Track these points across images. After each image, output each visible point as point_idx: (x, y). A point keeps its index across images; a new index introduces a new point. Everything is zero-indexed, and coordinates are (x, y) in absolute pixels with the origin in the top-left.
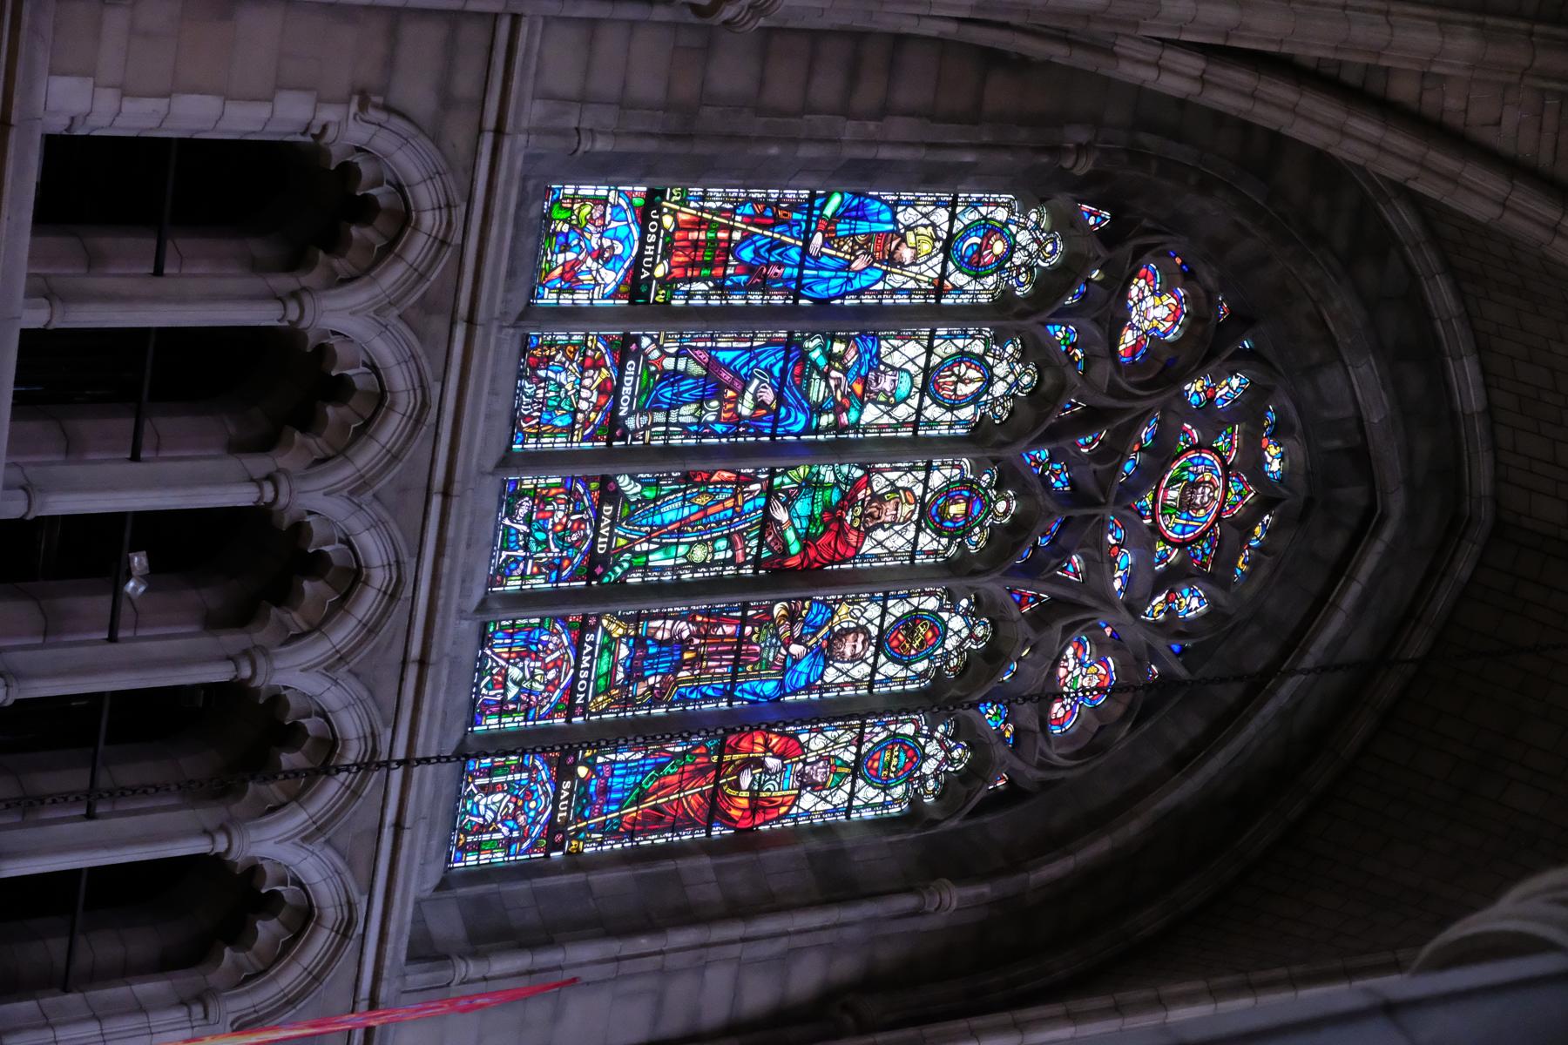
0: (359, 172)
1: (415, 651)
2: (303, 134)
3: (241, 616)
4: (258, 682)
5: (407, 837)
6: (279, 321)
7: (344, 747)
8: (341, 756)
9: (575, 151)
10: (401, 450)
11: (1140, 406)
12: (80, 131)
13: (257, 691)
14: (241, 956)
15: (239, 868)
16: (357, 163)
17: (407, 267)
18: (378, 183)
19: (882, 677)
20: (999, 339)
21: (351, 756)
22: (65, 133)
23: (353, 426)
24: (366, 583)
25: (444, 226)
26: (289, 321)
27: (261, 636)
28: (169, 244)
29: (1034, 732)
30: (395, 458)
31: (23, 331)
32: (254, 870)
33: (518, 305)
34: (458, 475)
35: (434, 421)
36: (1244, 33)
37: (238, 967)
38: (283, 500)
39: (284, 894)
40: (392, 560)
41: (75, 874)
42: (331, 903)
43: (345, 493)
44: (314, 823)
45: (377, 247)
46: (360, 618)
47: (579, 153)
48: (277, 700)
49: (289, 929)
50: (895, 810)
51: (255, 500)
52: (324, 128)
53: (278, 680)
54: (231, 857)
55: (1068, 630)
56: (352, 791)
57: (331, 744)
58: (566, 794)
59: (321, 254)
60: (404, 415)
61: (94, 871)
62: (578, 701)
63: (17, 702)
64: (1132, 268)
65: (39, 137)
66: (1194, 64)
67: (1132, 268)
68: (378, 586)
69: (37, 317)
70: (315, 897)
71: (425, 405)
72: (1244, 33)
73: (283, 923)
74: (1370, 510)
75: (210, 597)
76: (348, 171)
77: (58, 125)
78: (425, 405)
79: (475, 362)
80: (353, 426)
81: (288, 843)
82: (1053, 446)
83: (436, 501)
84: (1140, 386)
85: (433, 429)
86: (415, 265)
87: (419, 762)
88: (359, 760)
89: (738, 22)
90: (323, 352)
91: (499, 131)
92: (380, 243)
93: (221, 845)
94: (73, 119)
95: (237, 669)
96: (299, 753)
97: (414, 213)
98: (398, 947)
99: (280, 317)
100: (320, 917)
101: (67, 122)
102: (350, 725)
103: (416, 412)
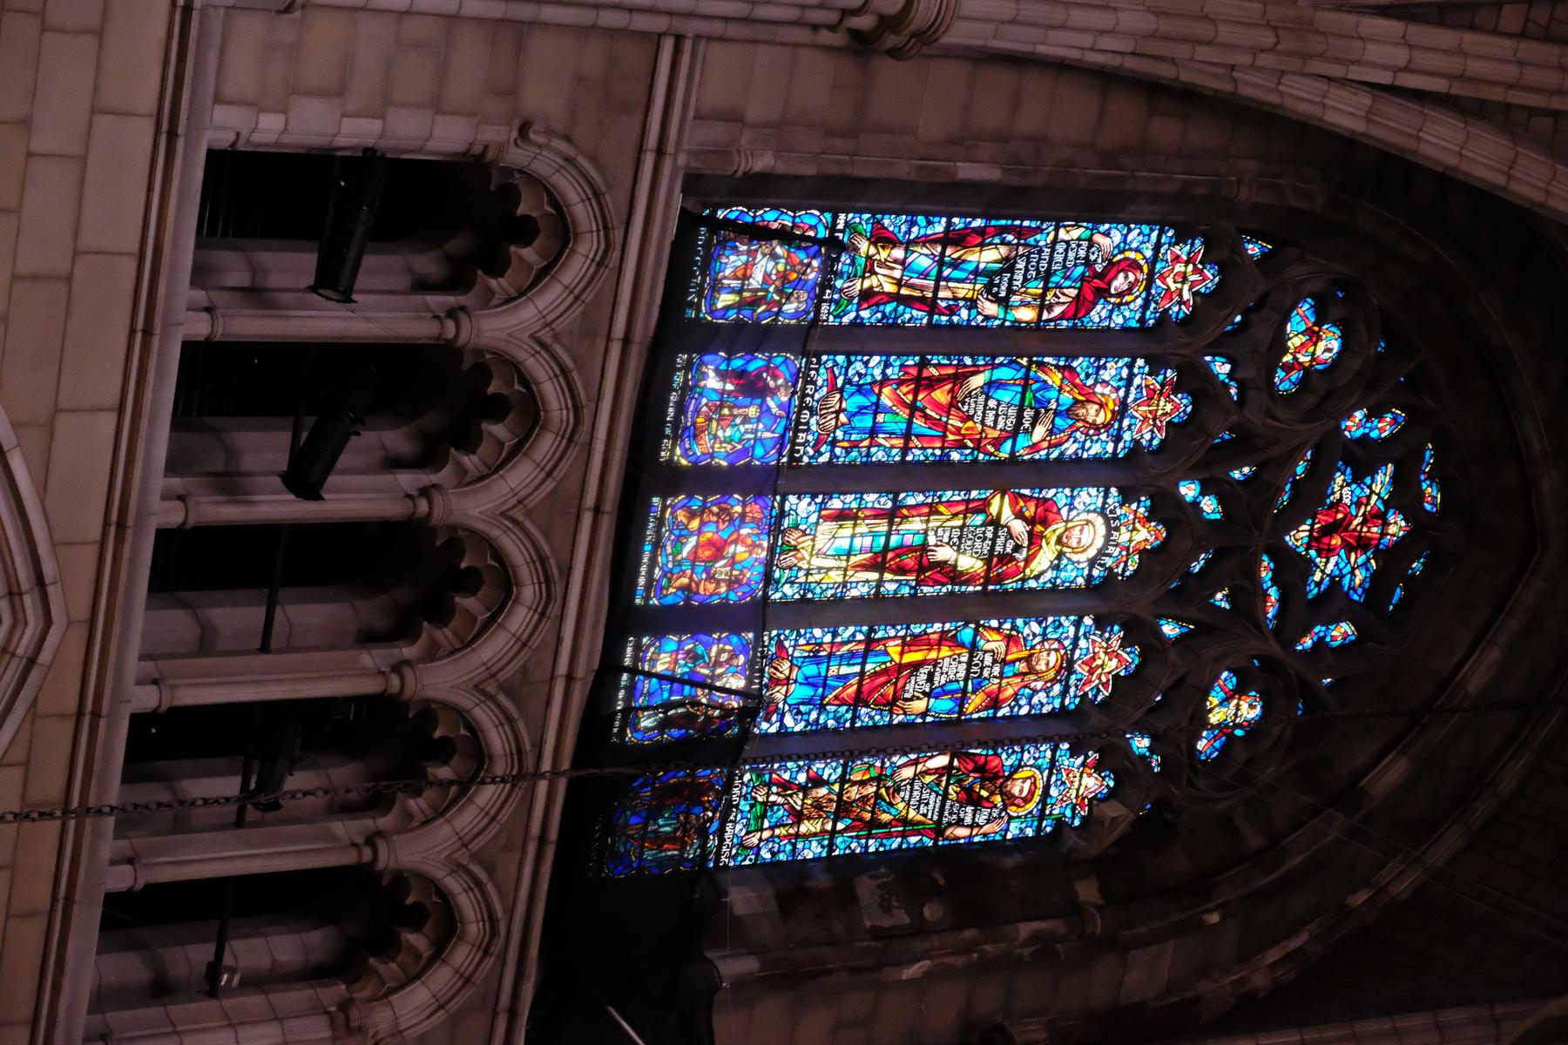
3: (457, 279)
4: (381, 865)
12: (241, 147)
13: (381, 874)
17: (535, 466)
19: (1054, 285)
25: (544, 599)
27: (445, 475)
35: (617, 265)
36: (1376, 118)
39: (428, 906)
42: (502, 752)
46: (513, 632)
49: (516, 436)
52: (486, 148)
57: (479, 754)
63: (149, 887)
65: (127, 717)
68: (528, 603)
71: (494, 932)
72: (1376, 118)
75: (428, 264)
76: (482, 371)
77: (224, 139)
86: (462, 970)
88: (508, 772)
91: (660, 152)
94: (238, 134)
96: (529, 248)
97: (542, 413)
100: (518, 597)
102: (497, 740)
103: (541, 574)
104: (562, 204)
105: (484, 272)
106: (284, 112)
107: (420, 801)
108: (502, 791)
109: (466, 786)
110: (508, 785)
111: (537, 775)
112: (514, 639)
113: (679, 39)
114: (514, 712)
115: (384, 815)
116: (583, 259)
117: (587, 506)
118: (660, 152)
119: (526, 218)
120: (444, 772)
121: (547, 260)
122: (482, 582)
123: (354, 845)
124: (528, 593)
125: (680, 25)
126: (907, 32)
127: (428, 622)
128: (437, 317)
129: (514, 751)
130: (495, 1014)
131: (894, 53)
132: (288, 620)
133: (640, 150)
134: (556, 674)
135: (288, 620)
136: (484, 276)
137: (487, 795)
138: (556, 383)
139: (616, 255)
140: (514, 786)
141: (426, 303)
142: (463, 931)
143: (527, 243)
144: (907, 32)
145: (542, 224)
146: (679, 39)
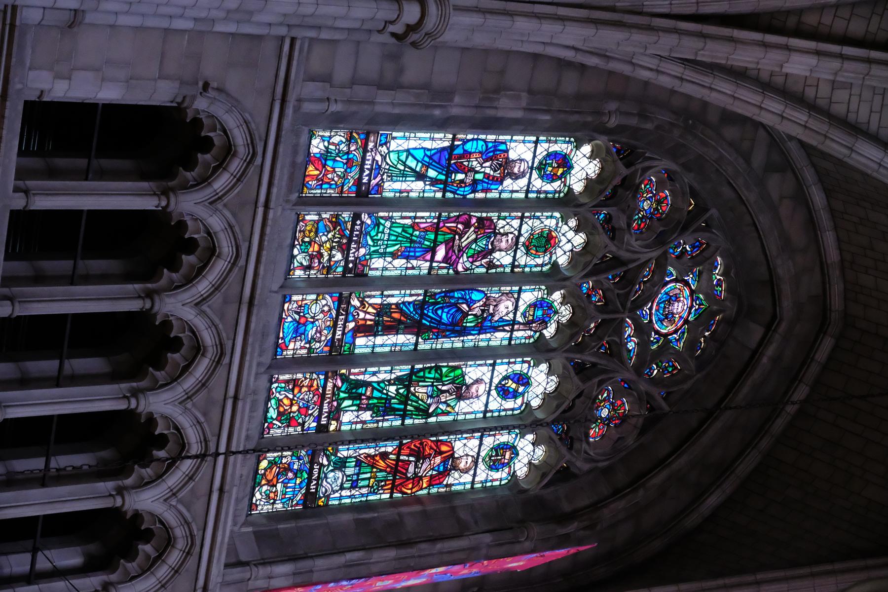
0: (187, 225)
1: (231, 392)
2: (172, 102)
3: (147, 274)
4: (140, 409)
5: (240, 404)
6: (156, 207)
7: (174, 541)
8: (188, 451)
9: (327, 110)
10: (193, 475)
11: (644, 258)
12: (46, 99)
14: (174, 276)
15: (143, 417)
16: (201, 118)
18: (214, 129)
20: (565, 220)
21: (195, 449)
22: (37, 100)
23: (212, 165)
24: (173, 546)
25: (219, 354)
26: (161, 207)
28: (53, 458)
29: (624, 230)
30: (191, 478)
31: (26, 102)
32: (137, 516)
33: (267, 359)
34: (258, 291)
37: (172, 282)
38: (156, 308)
39: (154, 530)
40: (202, 439)
41: (50, 418)
42: (243, 143)
43: (161, 500)
44: (187, 394)
45: (182, 365)
47: (329, 111)
48: (167, 324)
49: (158, 551)
50: (545, 269)
51: (141, 307)
53: (152, 408)
54: (124, 509)
55: (601, 383)
56: (237, 179)
58: (367, 172)
59: (165, 271)
60: (242, 159)
61: (61, 417)
62: (364, 181)
64: (641, 179)
65: (21, 107)
66: (676, 69)
67: (641, 179)
69: (19, 202)
70: (233, 140)
71: (238, 256)
73: (182, 356)
74: (774, 316)
78: (238, 256)
79: (247, 364)
80: (212, 165)
81: (156, 502)
82: (595, 278)
83: (260, 211)
84: (646, 247)
85: (258, 170)
87: (234, 453)
89: (419, 46)
90: (182, 225)
92: (154, 554)
93: (119, 502)
94: (42, 92)
95: (144, 303)
98: (220, 557)
99: (157, 204)
100: (219, 253)
101: (38, 93)
102: (192, 435)
104: (180, 427)
105: (183, 169)
106: (70, 79)
107: (148, 470)
108: (195, 464)
109: (173, 462)
110: (199, 460)
111: (217, 454)
112: (170, 569)
113: (293, 40)
114: (202, 419)
115: (113, 573)
116: (223, 262)
117: (277, 98)
118: (267, 206)
119: (161, 435)
120: (162, 454)
121: (202, 262)
122: (168, 441)
123: (111, 495)
124: (181, 544)
125: (295, 33)
126: (423, 32)
127: (168, 269)
128: (125, 397)
129: (218, 343)
130: (256, 207)
131: (414, 44)
132: (71, 366)
133: (211, 492)
134: (227, 396)
135: (71, 366)
136: (139, 469)
137: (186, 466)
138: (226, 233)
139: (197, 549)
140: (202, 461)
141: (134, 288)
142: (235, 151)
143: (147, 542)
144: (423, 32)
145: (170, 438)
146: (293, 40)
